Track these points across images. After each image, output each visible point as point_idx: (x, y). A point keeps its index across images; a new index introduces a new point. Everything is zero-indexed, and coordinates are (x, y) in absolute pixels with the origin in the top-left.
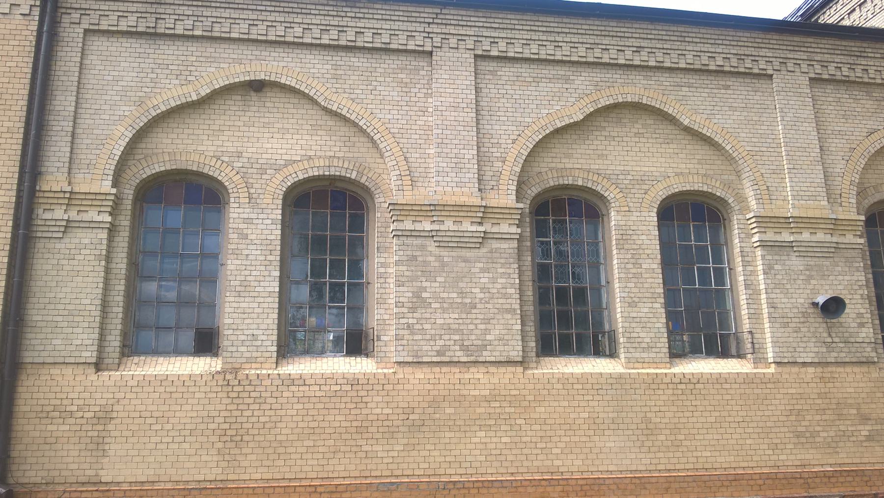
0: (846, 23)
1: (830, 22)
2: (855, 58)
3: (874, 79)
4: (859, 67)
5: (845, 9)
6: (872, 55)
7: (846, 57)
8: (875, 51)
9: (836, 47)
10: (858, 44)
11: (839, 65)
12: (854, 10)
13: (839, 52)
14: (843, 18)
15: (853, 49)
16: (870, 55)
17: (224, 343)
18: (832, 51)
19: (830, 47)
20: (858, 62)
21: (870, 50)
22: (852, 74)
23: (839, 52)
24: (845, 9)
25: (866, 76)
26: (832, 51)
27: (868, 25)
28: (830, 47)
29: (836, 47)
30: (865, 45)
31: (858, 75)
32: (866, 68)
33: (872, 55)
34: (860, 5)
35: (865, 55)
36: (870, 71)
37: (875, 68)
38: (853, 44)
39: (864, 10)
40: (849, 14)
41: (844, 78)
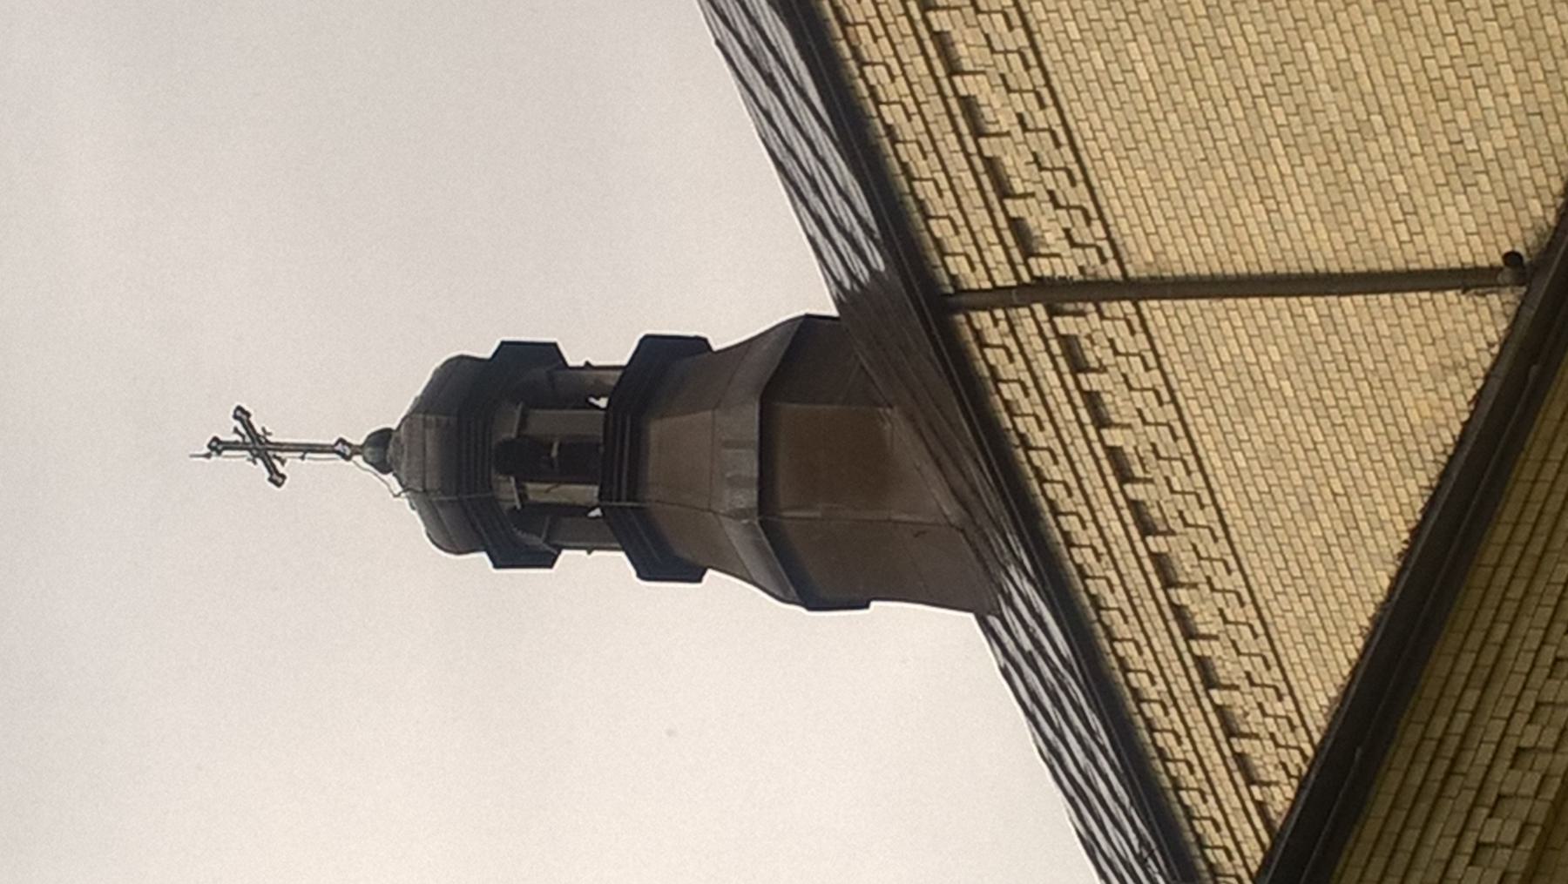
0: (1281, 798)
1: (1255, 855)
2: (1457, 781)
3: (1525, 826)
4: (1497, 774)
5: (1225, 789)
6: (1462, 719)
7: (1443, 813)
8: (1448, 704)
9: (1389, 840)
10: (1401, 757)
11: (1468, 847)
12: (1241, 758)
13: (1412, 835)
14: (1261, 806)
15: (1416, 779)
16: (1459, 726)
17: (387, 512)
18: (1402, 859)
19: (1379, 863)
20: (1477, 774)
21: (1440, 723)
22: (1523, 808)
23: (1412, 835)
24: (1225, 789)
25: (1543, 761)
26: (1402, 859)
27: (1318, 721)
28: (1379, 863)
29: (1389, 840)
30: (1412, 735)
31: (1529, 788)
32: (1508, 753)
33: (1462, 719)
34: (1231, 732)
35: (1453, 741)
36: (1489, 838)
37: (1520, 720)
38: (1394, 779)
39: (1254, 721)
40: (1250, 781)
41: (1529, 844)
